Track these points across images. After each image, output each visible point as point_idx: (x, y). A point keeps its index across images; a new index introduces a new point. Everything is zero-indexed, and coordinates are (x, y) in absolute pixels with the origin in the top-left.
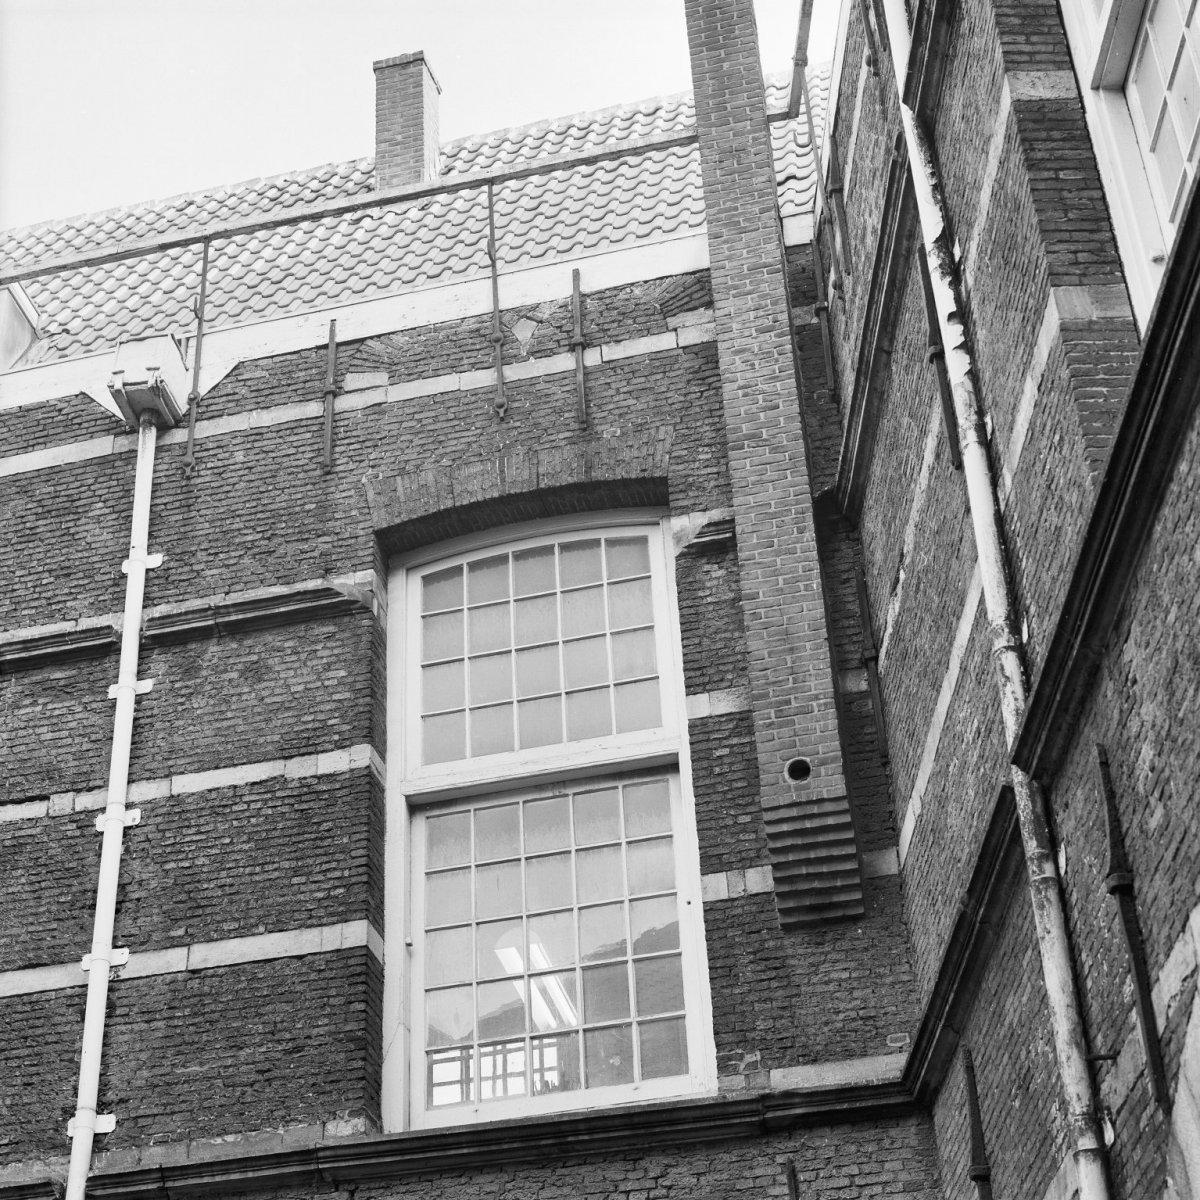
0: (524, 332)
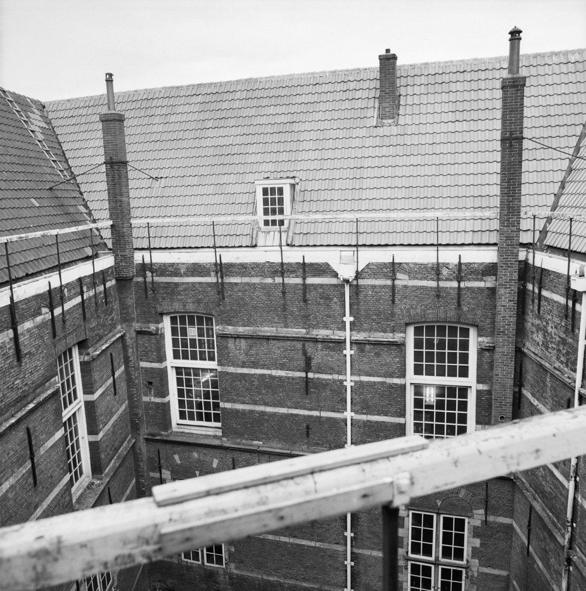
0: (445, 272)
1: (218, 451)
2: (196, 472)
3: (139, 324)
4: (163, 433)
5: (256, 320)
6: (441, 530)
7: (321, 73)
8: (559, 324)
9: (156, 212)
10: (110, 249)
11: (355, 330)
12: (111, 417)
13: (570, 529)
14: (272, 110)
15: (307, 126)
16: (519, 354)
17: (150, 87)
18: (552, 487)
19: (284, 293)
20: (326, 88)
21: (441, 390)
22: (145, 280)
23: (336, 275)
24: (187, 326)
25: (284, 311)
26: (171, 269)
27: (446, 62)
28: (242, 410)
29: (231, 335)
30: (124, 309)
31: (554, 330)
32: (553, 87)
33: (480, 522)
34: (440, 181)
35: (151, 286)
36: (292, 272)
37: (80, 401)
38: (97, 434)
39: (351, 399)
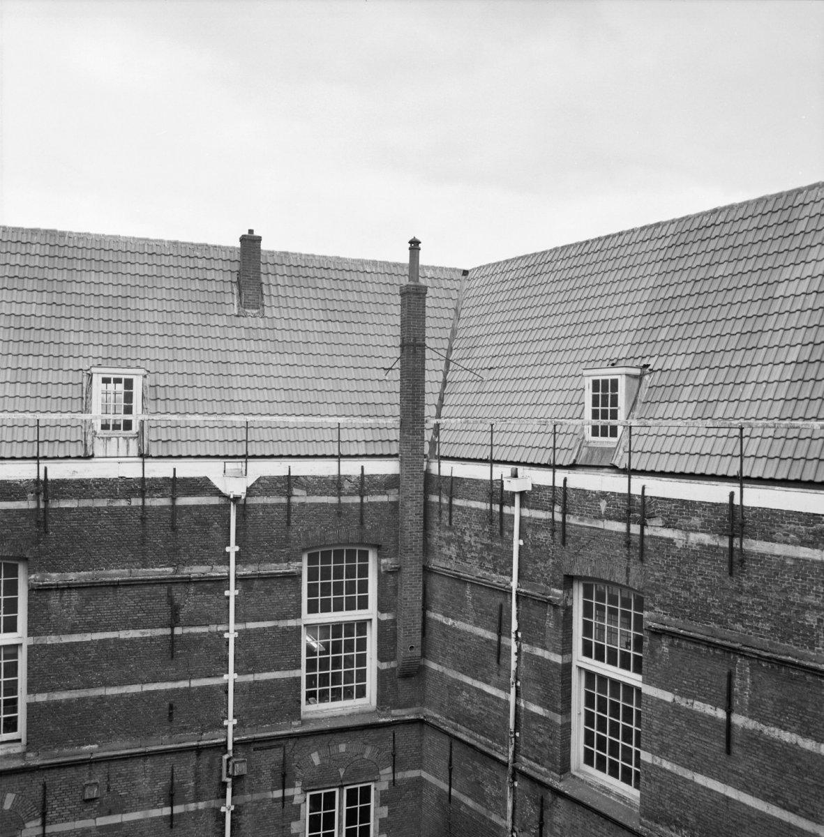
0: (347, 486)
13: (513, 739)
15: (148, 305)
18: (483, 706)
19: (143, 519)
27: (308, 255)
28: (66, 700)
33: (387, 783)
36: (156, 491)
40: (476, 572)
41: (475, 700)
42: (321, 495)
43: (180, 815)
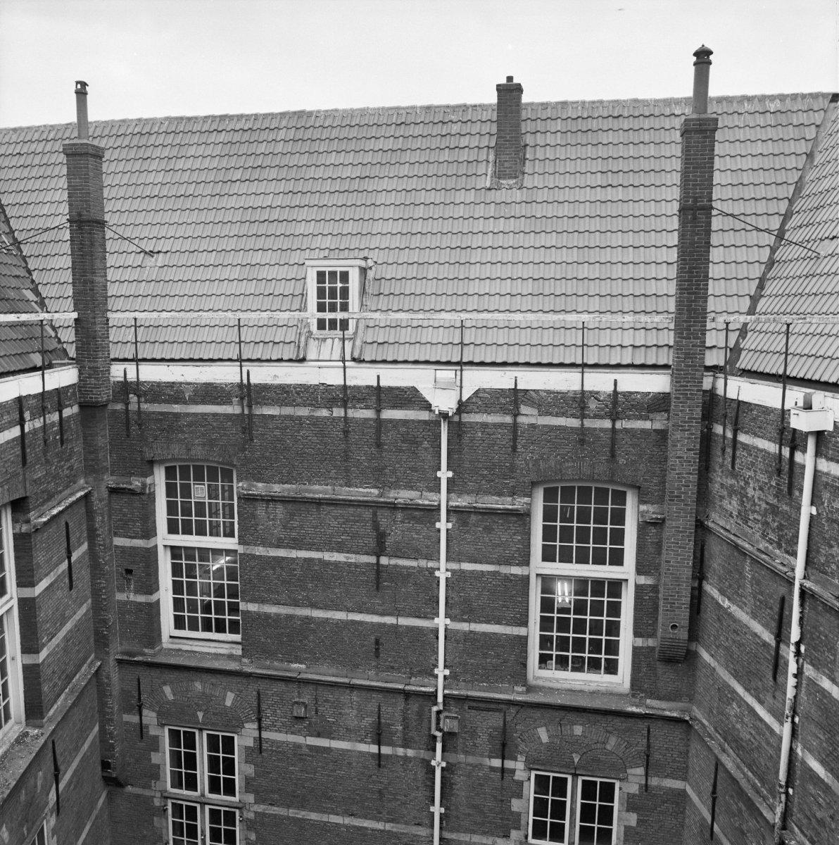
0: (593, 405)
1: (235, 680)
2: (198, 713)
3: (114, 478)
4: (146, 651)
5: (301, 474)
6: (579, 801)
7: (408, 108)
8: (766, 484)
9: (147, 304)
10: (73, 359)
11: (454, 491)
12: (62, 625)
13: (783, 797)
14: (332, 159)
15: (384, 184)
16: (701, 527)
17: (145, 116)
18: (753, 732)
19: (346, 432)
20: (418, 130)
21: (581, 585)
22: (127, 408)
23: (427, 406)
24: (192, 482)
25: (345, 461)
26: (168, 391)
28: (275, 614)
29: (261, 496)
30: (91, 453)
31: (758, 493)
32: (787, 116)
34: (584, 271)
35: (136, 417)
36: (359, 400)
37: (11, 598)
38: (37, 652)
39: (446, 598)
40: (757, 541)
41: (746, 720)
42: (557, 415)
43: (388, 756)
